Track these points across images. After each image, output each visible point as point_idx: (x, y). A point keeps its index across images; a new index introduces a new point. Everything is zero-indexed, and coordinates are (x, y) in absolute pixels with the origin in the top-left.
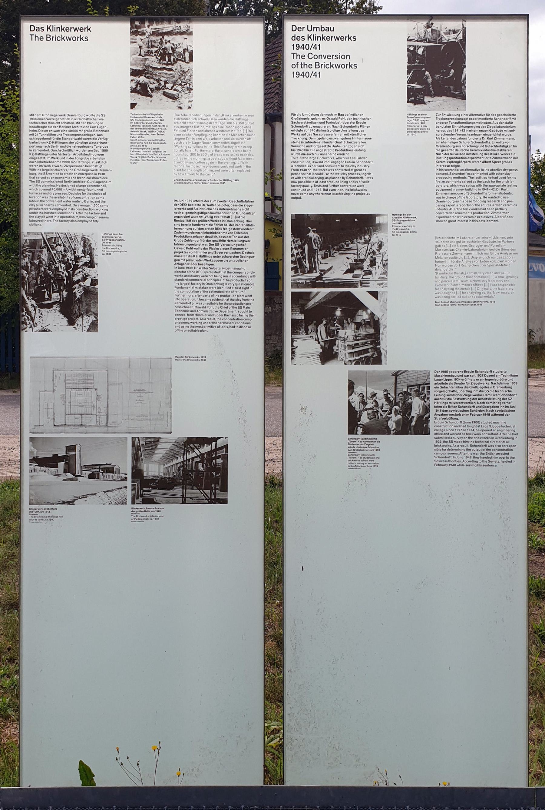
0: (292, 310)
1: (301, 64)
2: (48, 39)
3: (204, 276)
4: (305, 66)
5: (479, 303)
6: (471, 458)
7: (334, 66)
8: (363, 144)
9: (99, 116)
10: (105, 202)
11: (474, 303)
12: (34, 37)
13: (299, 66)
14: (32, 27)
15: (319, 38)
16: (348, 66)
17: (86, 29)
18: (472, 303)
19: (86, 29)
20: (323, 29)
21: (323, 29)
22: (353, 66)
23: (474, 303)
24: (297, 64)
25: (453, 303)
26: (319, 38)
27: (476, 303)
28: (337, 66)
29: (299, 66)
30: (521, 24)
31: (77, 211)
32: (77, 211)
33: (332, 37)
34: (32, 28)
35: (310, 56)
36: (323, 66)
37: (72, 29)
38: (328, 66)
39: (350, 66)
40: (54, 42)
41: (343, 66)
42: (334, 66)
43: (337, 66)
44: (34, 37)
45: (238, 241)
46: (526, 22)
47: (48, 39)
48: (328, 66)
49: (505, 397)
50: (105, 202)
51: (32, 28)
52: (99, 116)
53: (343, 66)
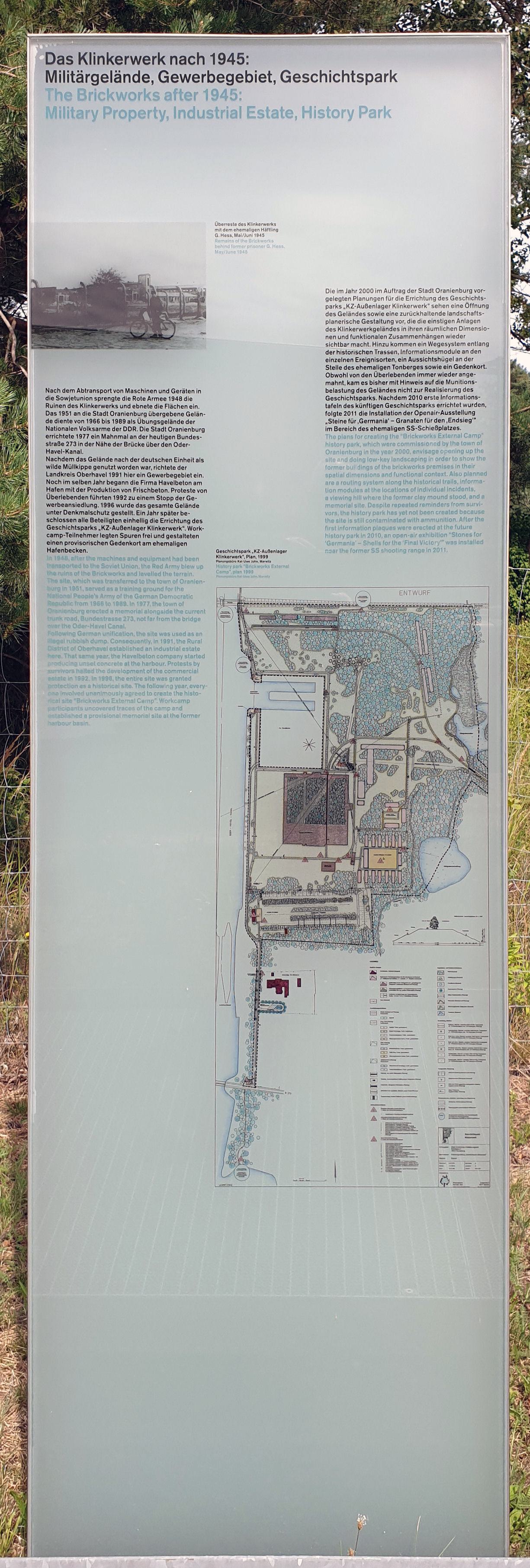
0: (26, 525)
3: (404, 528)
7: (114, 96)
10: (482, 451)
13: (162, 96)
15: (101, 60)
16: (142, 97)
19: (156, 60)
20: (211, 78)
21: (211, 78)
26: (101, 60)
29: (162, 96)
31: (463, 516)
32: (463, 516)
33: (126, 58)
36: (93, 97)
37: (129, 60)
38: (337, 78)
42: (114, 96)
44: (53, 93)
45: (463, 412)
47: (82, 97)
48: (102, 97)
49: (181, 495)
50: (482, 451)
53: (132, 97)
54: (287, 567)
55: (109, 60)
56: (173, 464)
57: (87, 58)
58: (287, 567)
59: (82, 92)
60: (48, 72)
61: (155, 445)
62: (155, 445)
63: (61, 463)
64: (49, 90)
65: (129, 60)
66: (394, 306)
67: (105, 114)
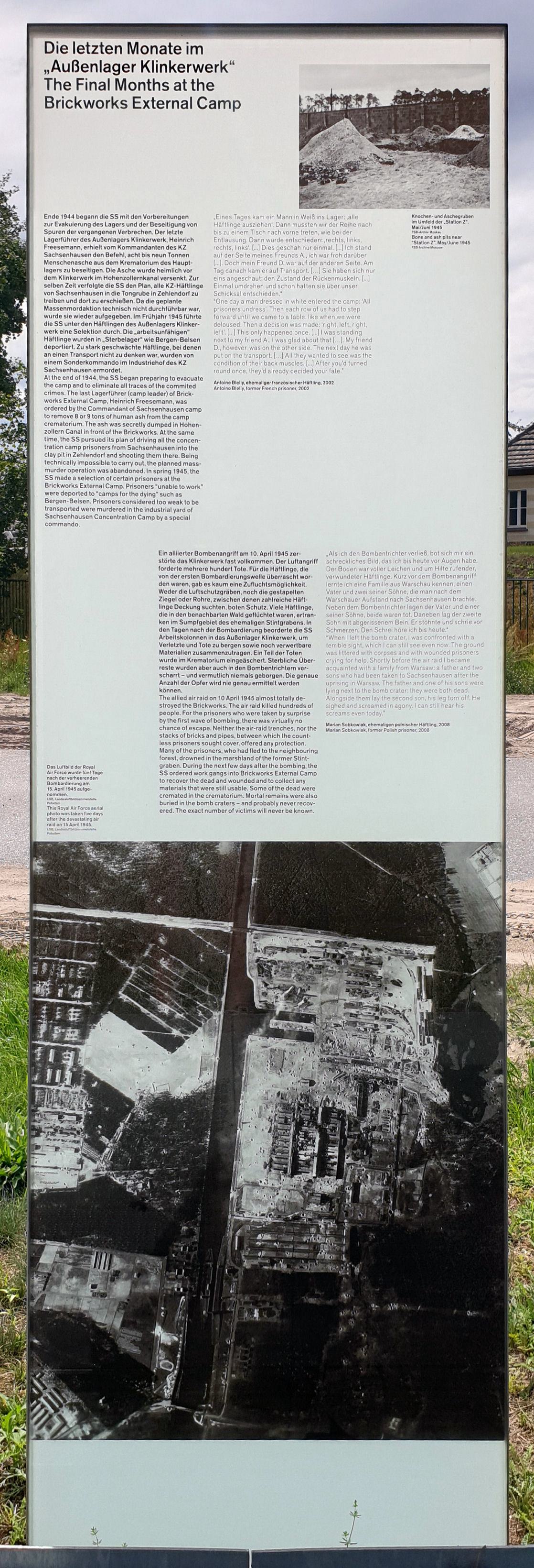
1: (193, 83)
2: (49, 105)
4: (157, 86)
5: (302, 385)
6: (89, 416)
7: (82, 104)
8: (191, 390)
9: (106, 217)
11: (292, 386)
12: (52, 82)
13: (189, 86)
14: (49, 45)
17: (219, 68)
18: (289, 386)
19: (219, 68)
22: (118, 104)
23: (292, 386)
24: (184, 82)
25: (252, 385)
27: (297, 386)
28: (89, 104)
29: (189, 86)
30: (495, 44)
34: (49, 46)
35: (203, 103)
36: (60, 104)
37: (191, 68)
39: (114, 104)
40: (60, 111)
41: (100, 104)
42: (82, 104)
43: (89, 104)
44: (52, 82)
46: (503, 40)
47: (49, 105)
48: (69, 104)
51: (49, 46)
52: (106, 217)
53: (100, 104)
54: (316, 676)
55: (172, 68)
56: (283, 808)
57: (150, 65)
58: (316, 676)
59: (49, 100)
60: (129, 44)
61: (223, 811)
62: (223, 811)
63: (199, 573)
64: (48, 79)
65: (191, 68)
66: (144, 66)
67: (78, 84)
